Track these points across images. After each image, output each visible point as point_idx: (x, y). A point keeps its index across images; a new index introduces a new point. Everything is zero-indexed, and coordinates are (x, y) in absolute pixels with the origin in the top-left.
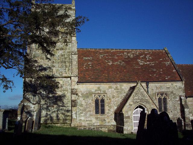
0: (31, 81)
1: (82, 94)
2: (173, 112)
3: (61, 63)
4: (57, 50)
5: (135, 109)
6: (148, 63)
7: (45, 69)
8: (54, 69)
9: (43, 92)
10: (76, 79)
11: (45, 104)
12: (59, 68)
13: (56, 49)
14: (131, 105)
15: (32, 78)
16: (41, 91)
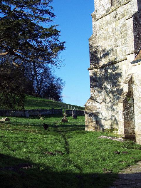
0: (95, 74)
3: (123, 38)
4: (118, 19)
7: (106, 54)
8: (118, 49)
10: (132, 58)
11: (110, 101)
12: (122, 46)
13: (117, 19)
15: (98, 69)
16: (105, 84)
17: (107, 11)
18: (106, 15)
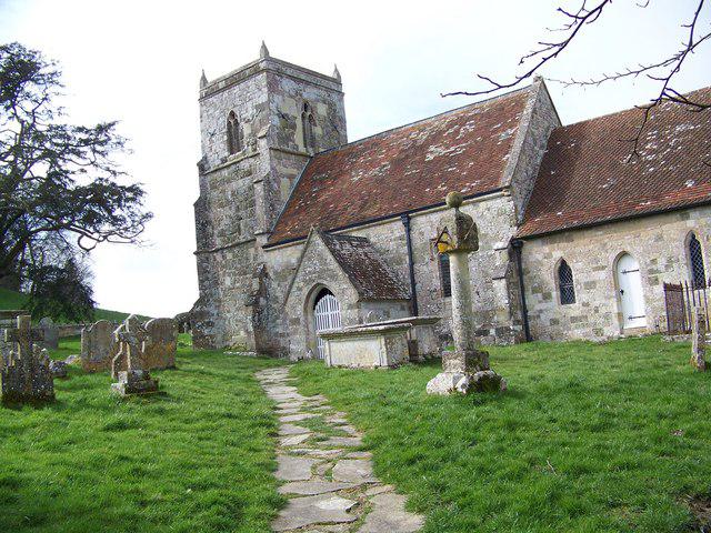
1: (276, 273)
2: (482, 294)
5: (316, 304)
6: (452, 149)
9: (690, 477)
14: (300, 289)
17: (224, 160)
18: (417, 280)
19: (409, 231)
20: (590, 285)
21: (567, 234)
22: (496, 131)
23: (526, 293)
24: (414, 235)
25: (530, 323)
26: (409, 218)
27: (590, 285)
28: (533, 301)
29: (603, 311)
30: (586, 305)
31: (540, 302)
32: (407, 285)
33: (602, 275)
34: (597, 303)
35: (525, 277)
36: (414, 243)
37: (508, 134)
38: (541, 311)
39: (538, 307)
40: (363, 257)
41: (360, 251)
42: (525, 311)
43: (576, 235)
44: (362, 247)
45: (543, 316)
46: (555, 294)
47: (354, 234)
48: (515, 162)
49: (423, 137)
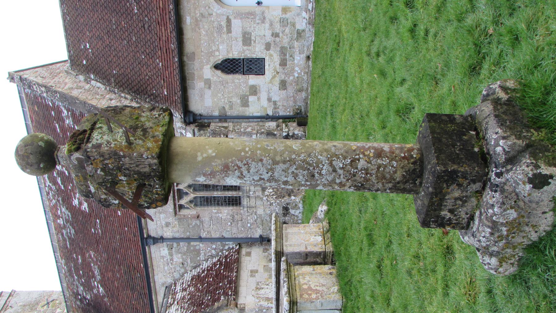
19: (162, 239)
20: (247, 39)
21: (185, 59)
22: (62, 128)
23: (247, 114)
24: (168, 234)
25: (281, 113)
26: (149, 237)
27: (247, 39)
28: (254, 109)
29: (278, 28)
30: (268, 47)
31: (259, 99)
32: (224, 246)
33: (237, 24)
34: (268, 33)
35: (229, 113)
36: (177, 235)
37: (68, 117)
38: (269, 100)
39: (264, 102)
40: (553, 309)
41: (179, 296)
42: (267, 118)
43: (189, 47)
44: (175, 293)
45: (275, 98)
46: (253, 80)
47: (160, 299)
48: (297, 293)
49: (63, 210)
